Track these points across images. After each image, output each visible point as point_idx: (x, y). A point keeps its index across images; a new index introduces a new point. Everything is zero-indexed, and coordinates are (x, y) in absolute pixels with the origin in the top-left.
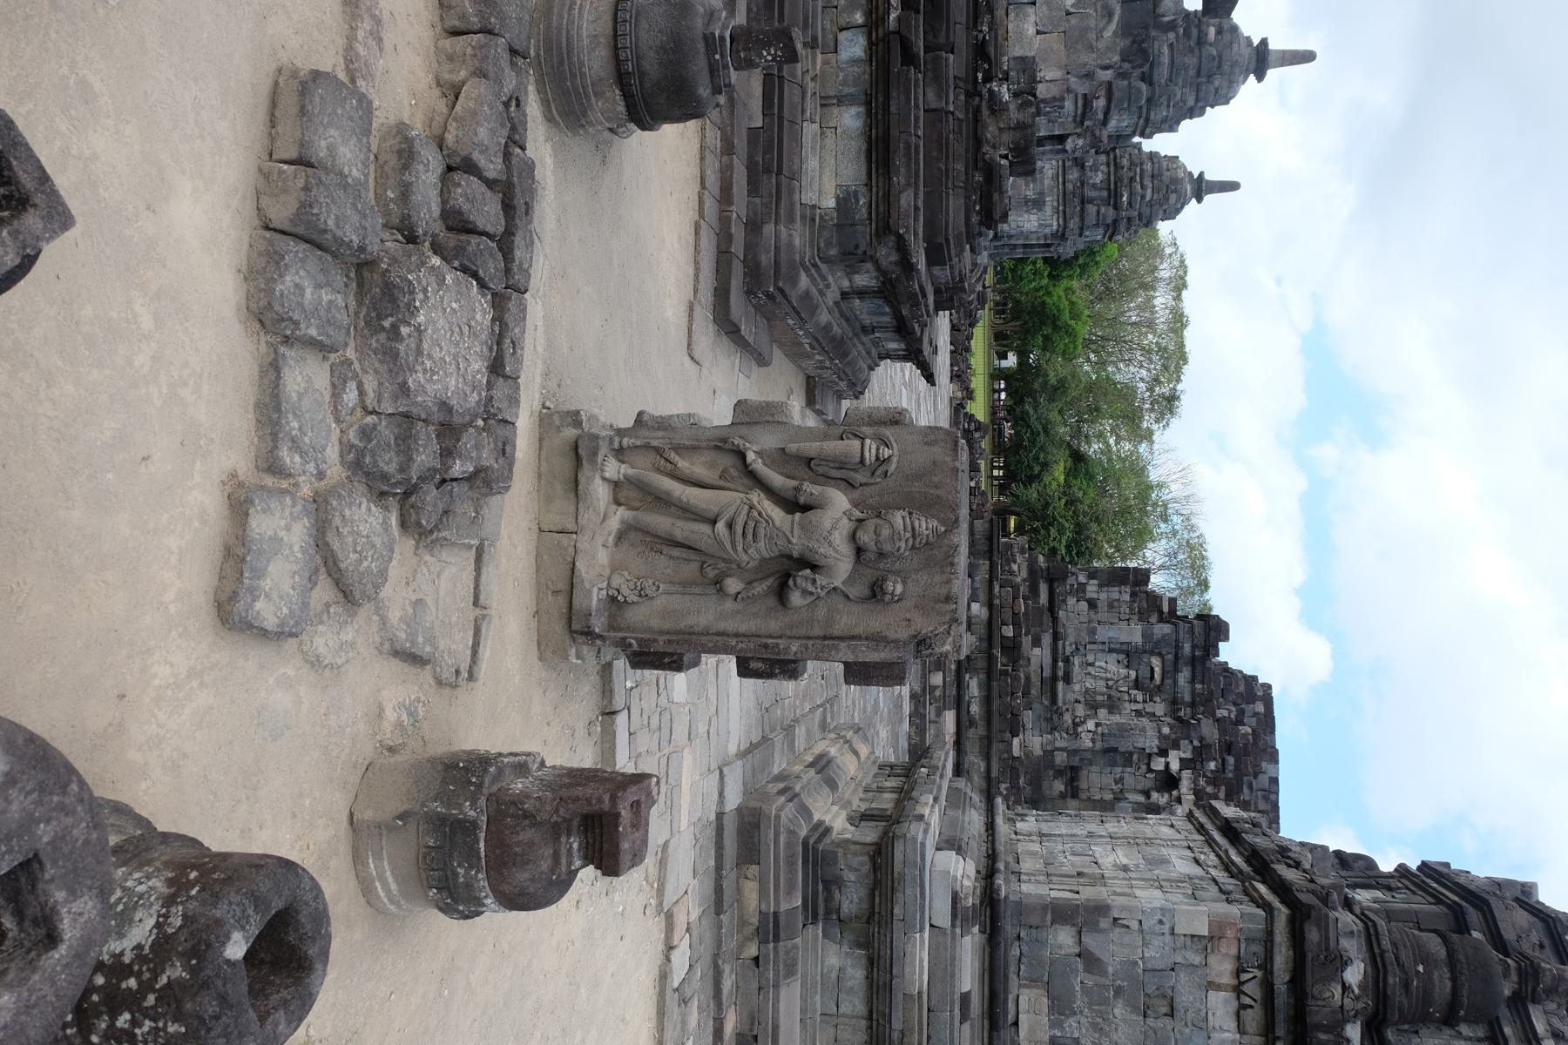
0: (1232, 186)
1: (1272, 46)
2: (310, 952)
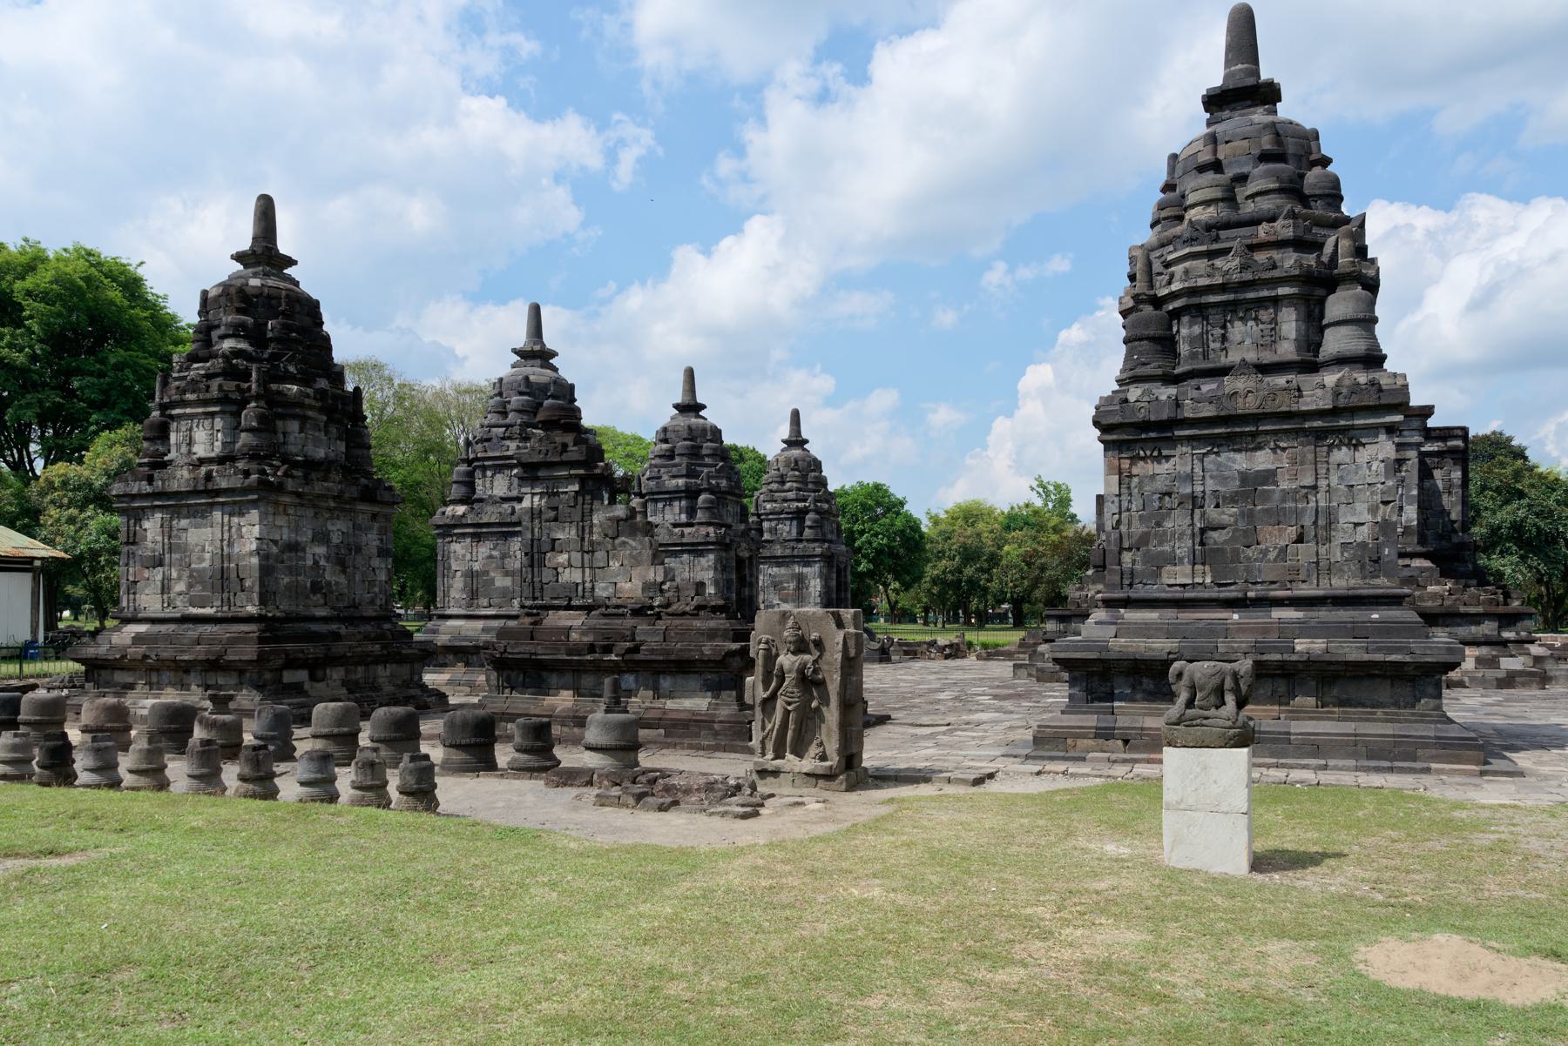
1: (679, 400)
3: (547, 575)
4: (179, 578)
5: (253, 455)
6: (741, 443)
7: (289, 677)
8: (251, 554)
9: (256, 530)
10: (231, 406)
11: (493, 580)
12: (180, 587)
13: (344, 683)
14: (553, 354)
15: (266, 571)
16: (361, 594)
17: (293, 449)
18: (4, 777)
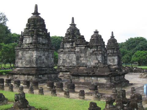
0: (73, 19)
2: (101, 100)
3: (80, 61)
4: (24, 61)
5: (35, 43)
6: (65, 32)
7: (40, 76)
8: (34, 58)
9: (35, 54)
10: (32, 36)
11: (67, 61)
12: (24, 63)
13: (47, 77)
14: (76, 25)
15: (37, 60)
16: (49, 64)
17: (40, 42)
18: (1, 88)
